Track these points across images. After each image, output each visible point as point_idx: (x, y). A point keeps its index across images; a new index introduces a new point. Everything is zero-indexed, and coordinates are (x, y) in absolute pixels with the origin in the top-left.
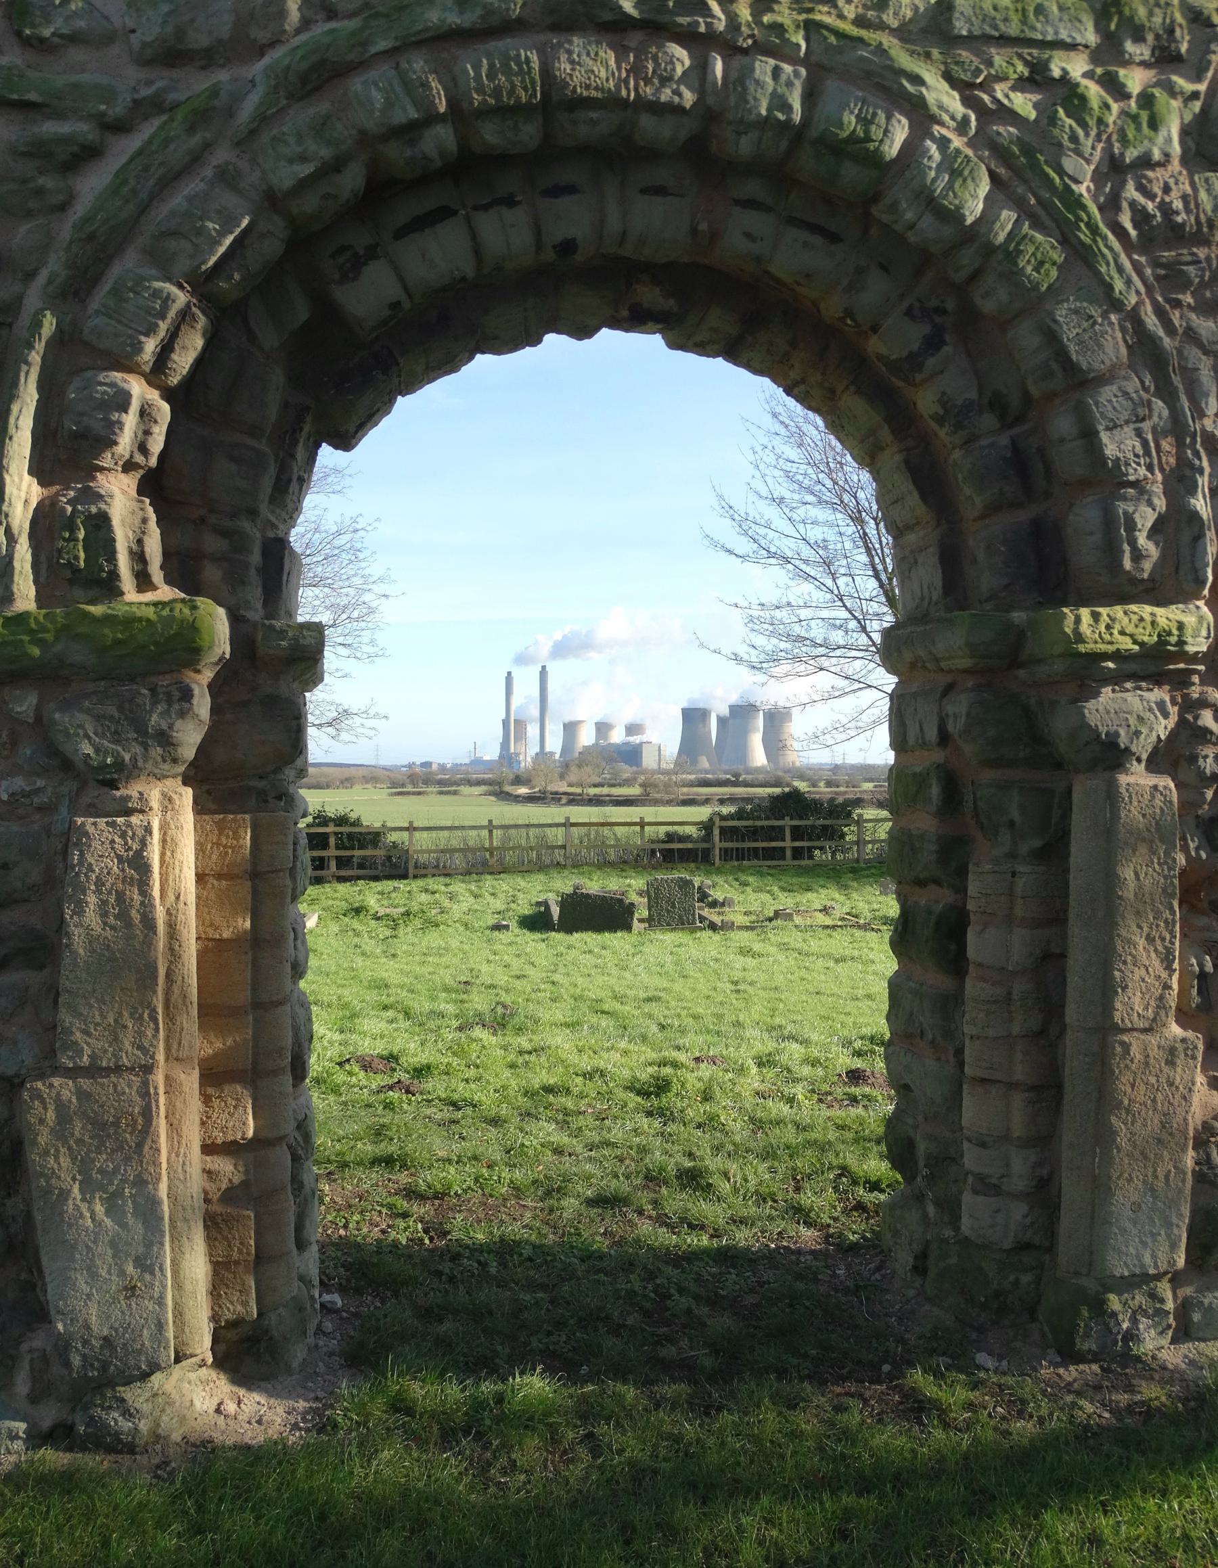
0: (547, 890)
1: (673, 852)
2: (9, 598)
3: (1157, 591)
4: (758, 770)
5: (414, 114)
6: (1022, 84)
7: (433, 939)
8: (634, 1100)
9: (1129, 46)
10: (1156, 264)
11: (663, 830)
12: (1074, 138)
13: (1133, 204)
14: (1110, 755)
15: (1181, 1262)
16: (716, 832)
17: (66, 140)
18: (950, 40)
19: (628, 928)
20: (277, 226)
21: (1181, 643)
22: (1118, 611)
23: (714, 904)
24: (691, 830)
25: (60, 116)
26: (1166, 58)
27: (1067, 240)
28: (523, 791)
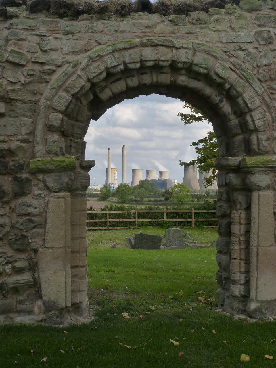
17: (50, 70)
19: (159, 248)
20: (88, 85)
25: (48, 65)
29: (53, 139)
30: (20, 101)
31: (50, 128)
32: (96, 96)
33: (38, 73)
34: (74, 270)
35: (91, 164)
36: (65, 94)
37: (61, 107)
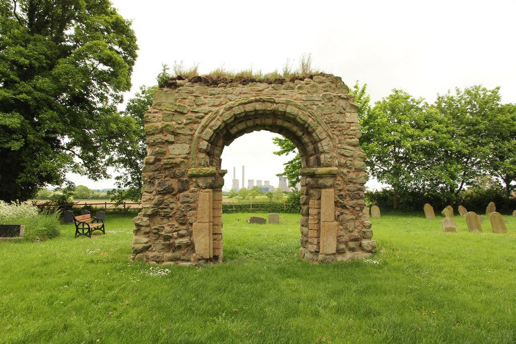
20: (223, 124)
29: (202, 156)
30: (183, 134)
31: (201, 151)
32: (228, 132)
33: (194, 118)
34: (214, 236)
35: (225, 172)
36: (210, 130)
37: (208, 138)
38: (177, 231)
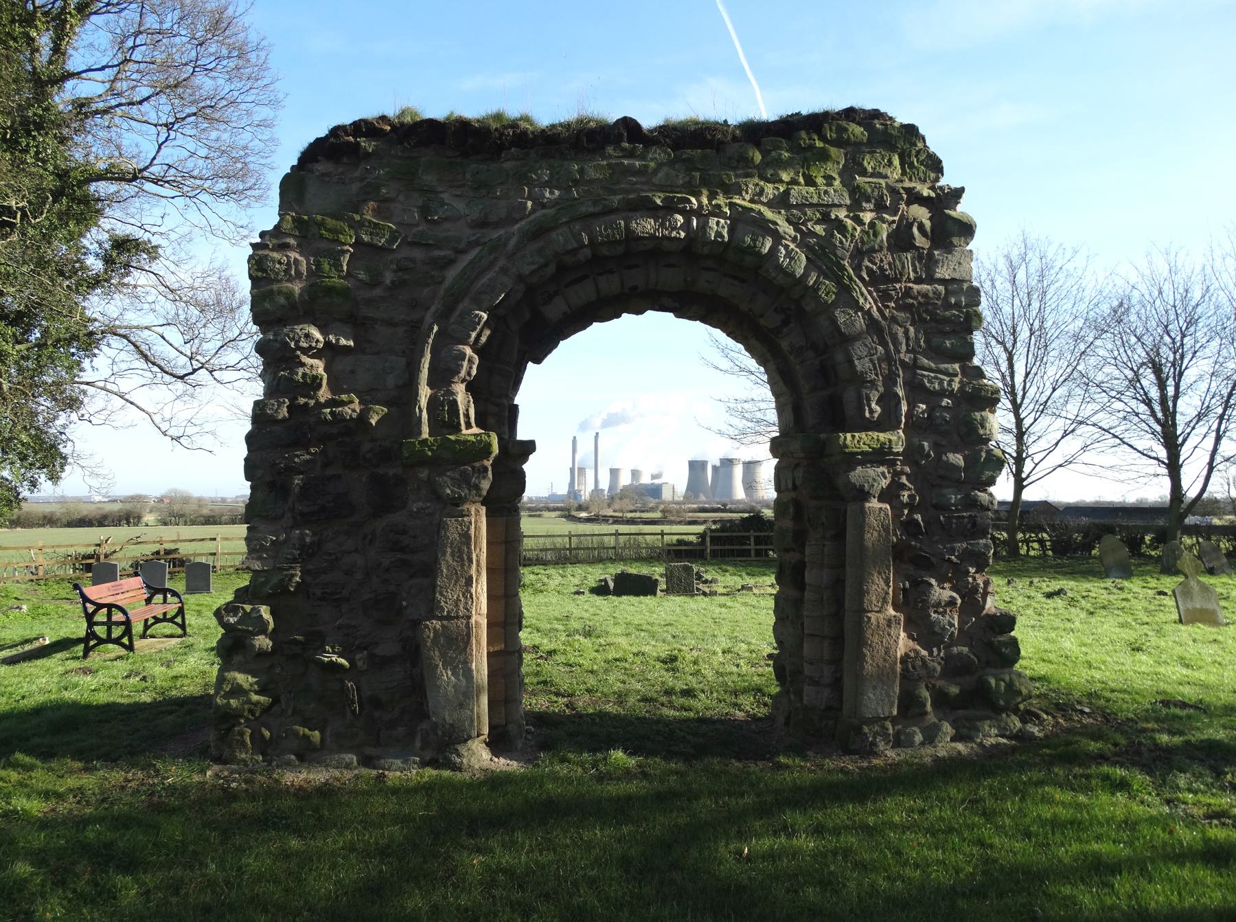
0: (608, 573)
1: (680, 552)
2: (420, 433)
3: (879, 426)
4: (739, 502)
5: (575, 245)
6: (818, 222)
7: (540, 598)
8: (658, 665)
9: (864, 204)
10: (877, 291)
11: (675, 538)
12: (841, 242)
13: (867, 267)
14: (863, 495)
15: (895, 713)
16: (708, 539)
18: (788, 207)
19: (655, 594)
21: (890, 448)
22: (863, 435)
23: (706, 582)
24: (693, 538)
25: (440, 248)
26: (880, 207)
27: (839, 281)
28: (584, 515)
38: (365, 648)
